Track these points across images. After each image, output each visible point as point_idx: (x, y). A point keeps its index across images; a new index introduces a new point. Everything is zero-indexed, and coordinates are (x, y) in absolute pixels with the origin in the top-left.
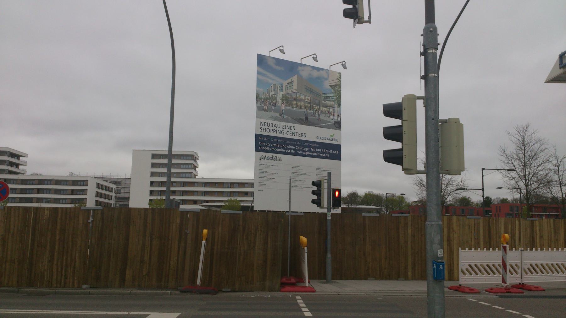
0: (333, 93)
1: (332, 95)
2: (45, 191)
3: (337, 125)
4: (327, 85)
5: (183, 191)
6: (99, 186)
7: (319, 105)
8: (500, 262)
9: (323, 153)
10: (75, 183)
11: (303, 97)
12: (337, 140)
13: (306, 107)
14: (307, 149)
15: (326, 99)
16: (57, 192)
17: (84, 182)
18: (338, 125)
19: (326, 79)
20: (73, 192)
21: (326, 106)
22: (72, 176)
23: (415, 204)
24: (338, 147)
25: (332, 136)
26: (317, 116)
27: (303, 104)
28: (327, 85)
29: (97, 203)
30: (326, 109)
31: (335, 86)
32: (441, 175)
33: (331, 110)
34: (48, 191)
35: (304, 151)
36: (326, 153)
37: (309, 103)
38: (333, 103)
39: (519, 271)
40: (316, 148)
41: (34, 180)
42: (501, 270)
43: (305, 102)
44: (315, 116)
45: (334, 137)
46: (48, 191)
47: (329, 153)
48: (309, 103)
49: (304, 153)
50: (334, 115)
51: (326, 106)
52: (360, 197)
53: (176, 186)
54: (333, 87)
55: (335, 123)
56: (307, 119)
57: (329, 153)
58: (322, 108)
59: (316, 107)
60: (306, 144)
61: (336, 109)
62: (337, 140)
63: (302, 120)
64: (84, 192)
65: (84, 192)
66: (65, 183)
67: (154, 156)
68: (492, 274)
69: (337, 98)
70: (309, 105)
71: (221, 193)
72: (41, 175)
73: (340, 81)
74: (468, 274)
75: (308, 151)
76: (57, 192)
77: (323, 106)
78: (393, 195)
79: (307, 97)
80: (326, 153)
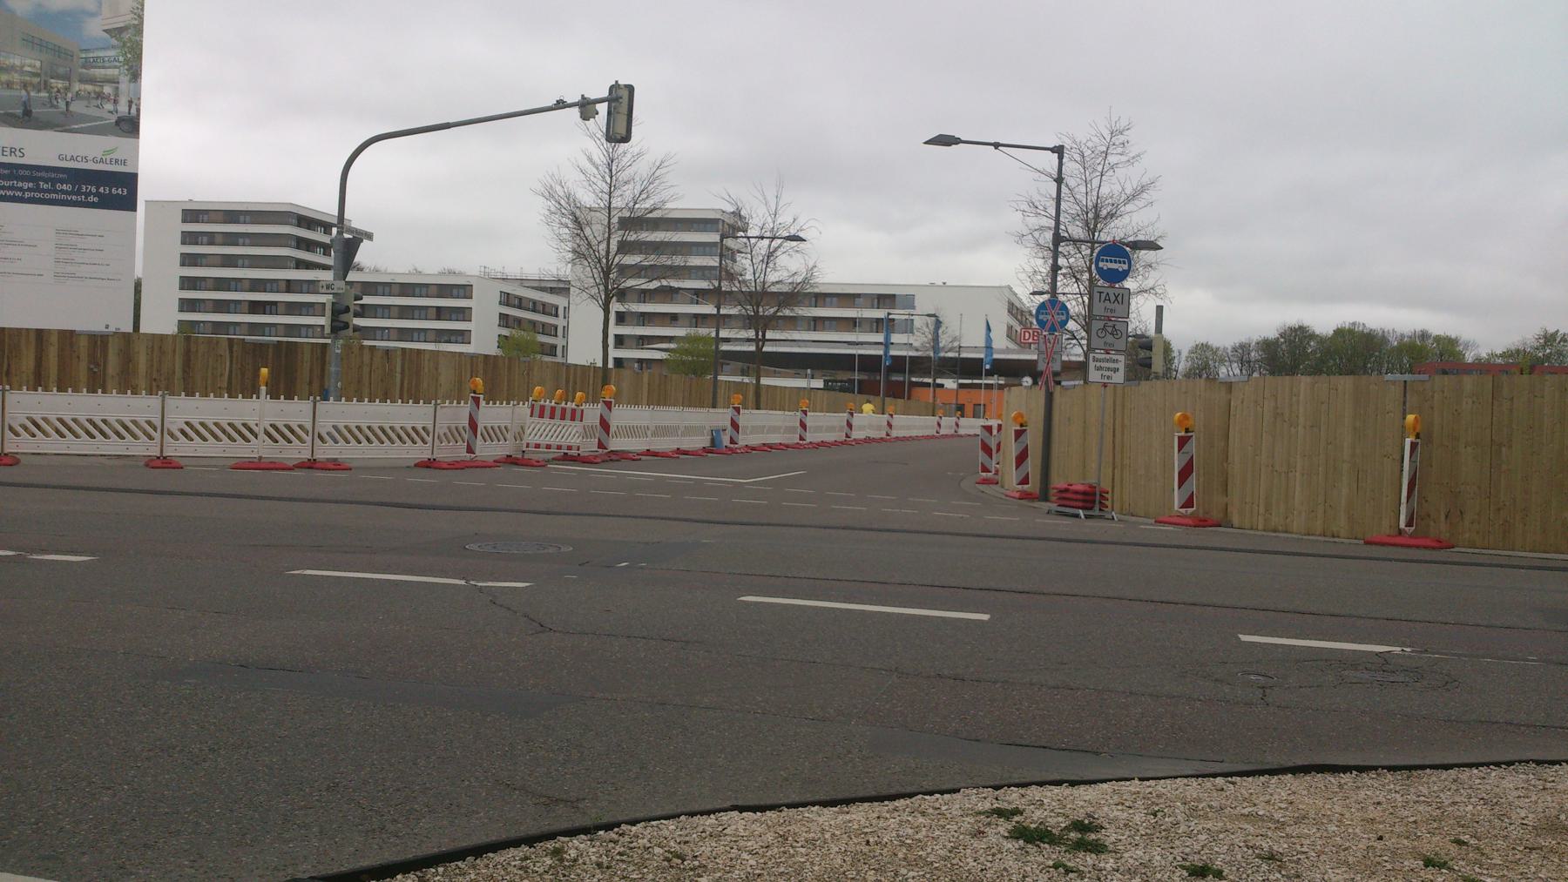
0: (113, 47)
1: (112, 53)
2: (380, 311)
3: (125, 126)
4: (95, 28)
5: (696, 316)
6: (507, 299)
7: (67, 77)
8: (466, 422)
9: (79, 193)
10: (444, 290)
11: (17, 62)
12: (124, 162)
13: (25, 86)
14: (26, 185)
15: (87, 64)
16: (405, 312)
17: (465, 290)
18: (129, 126)
19: (93, 15)
20: (440, 313)
21: (92, 81)
22: (441, 274)
23: (1499, 361)
24: (130, 181)
25: (112, 151)
26: (62, 105)
27: (16, 77)
28: (95, 28)
29: (503, 341)
30: (89, 88)
31: (121, 30)
32: (346, 236)
33: (107, 89)
34: (421, 312)
35: (21, 189)
36: (87, 194)
37: (37, 75)
38: (116, 72)
39: (429, 439)
40: (54, 181)
41: (427, 285)
42: (466, 437)
43: (22, 72)
44: (53, 106)
45: (114, 156)
46: (421, 312)
47: (97, 194)
48: (37, 75)
49: (19, 194)
50: (116, 102)
51: (92, 81)
52: (1321, 340)
53: (831, 306)
54: (116, 32)
55: (119, 122)
56: (27, 113)
57: (97, 194)
58: (77, 87)
59: (60, 84)
60: (27, 173)
61: (123, 87)
62: (124, 162)
63: (12, 115)
64: (463, 314)
65: (463, 314)
66: (424, 291)
67: (191, 215)
68: (387, 442)
69: (127, 62)
70: (36, 80)
71: (852, 324)
72: (460, 274)
73: (141, 17)
74: (330, 442)
75: (29, 190)
76: (405, 312)
77: (82, 81)
78: (1424, 335)
79: (28, 61)
80: (87, 194)
